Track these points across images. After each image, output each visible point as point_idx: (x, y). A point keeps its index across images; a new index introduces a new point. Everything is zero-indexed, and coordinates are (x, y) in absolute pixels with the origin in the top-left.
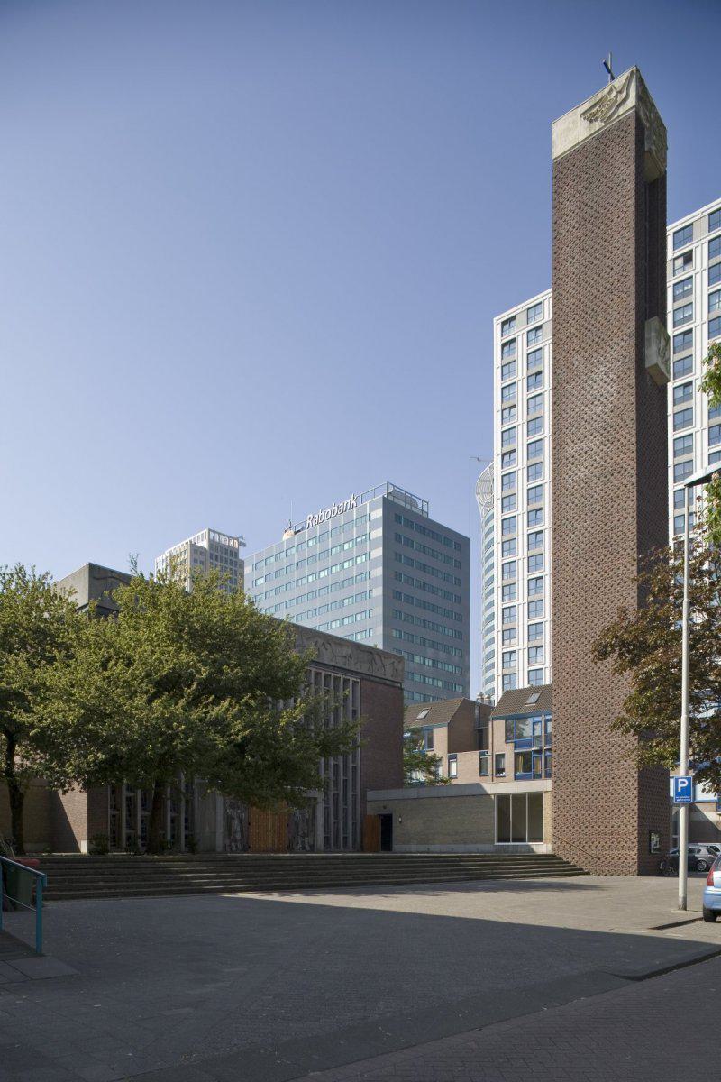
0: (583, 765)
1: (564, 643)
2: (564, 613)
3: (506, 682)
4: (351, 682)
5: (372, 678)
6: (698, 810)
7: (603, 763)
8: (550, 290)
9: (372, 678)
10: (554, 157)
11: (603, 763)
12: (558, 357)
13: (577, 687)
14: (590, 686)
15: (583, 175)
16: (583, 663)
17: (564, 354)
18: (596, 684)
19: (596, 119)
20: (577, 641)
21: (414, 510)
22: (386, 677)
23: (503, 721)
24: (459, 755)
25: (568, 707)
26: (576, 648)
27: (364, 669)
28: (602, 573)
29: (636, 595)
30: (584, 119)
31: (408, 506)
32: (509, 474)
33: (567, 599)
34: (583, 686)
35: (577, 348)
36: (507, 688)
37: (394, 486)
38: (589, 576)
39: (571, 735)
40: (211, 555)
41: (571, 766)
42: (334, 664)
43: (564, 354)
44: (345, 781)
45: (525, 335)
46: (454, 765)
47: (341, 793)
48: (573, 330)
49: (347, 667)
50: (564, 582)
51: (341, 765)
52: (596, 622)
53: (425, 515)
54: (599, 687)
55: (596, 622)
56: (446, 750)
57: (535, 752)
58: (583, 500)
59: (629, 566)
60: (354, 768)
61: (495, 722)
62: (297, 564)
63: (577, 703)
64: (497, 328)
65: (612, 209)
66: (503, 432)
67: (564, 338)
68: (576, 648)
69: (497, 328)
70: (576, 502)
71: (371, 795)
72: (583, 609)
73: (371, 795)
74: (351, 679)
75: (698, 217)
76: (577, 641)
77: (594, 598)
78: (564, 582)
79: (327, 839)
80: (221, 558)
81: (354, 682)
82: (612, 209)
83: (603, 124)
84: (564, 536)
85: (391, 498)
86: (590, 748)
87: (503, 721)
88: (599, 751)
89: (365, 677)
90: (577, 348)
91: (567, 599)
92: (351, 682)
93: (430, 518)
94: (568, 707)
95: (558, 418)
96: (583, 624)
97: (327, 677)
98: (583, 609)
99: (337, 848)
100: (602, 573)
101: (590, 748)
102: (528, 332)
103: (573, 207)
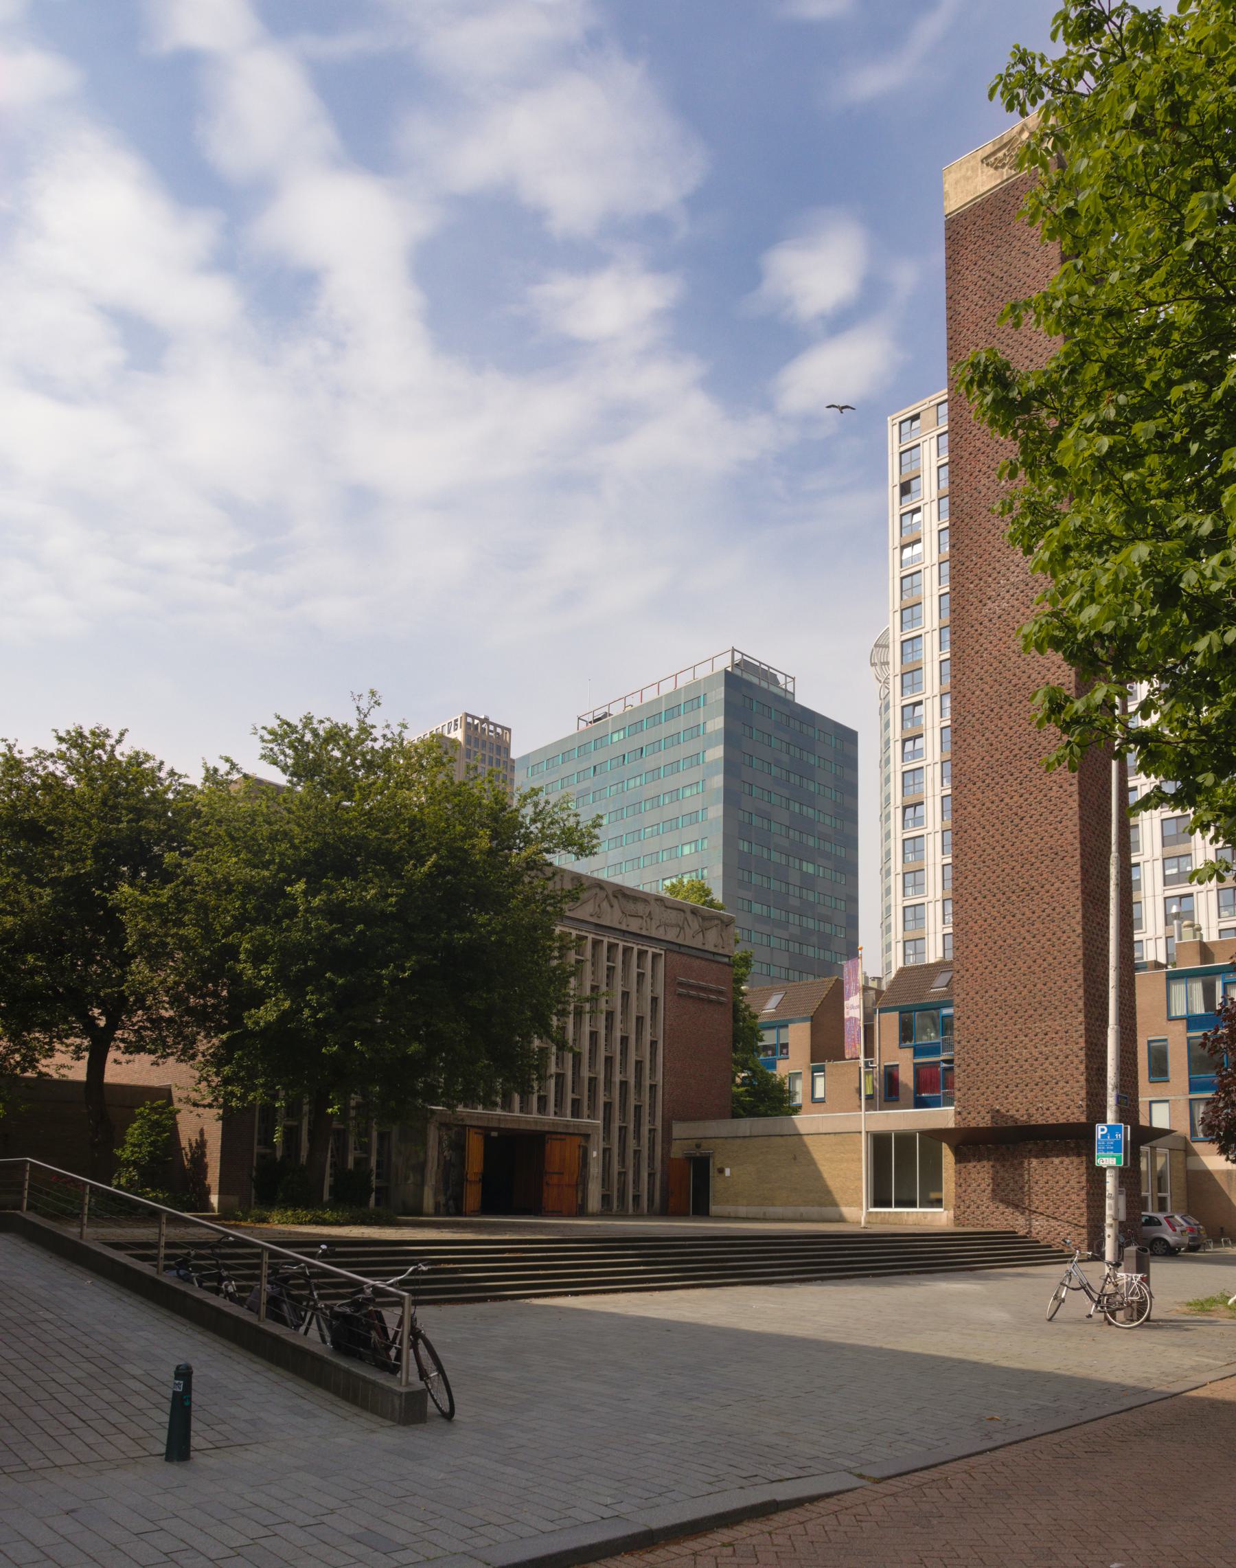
0: (1002, 1087)
1: (970, 900)
2: (970, 854)
3: (909, 952)
4: (650, 955)
5: (682, 950)
6: (1195, 1154)
7: (1032, 1085)
8: (946, 390)
9: (682, 950)
10: (947, 212)
11: (1032, 1085)
12: (958, 481)
13: (991, 968)
14: (1010, 965)
15: (988, 237)
16: (999, 930)
17: (966, 477)
18: (1020, 963)
19: (1004, 166)
20: (989, 897)
21: (773, 689)
22: (706, 948)
23: (896, 1014)
24: (828, 1065)
25: (977, 998)
26: (988, 908)
27: (671, 935)
28: (1026, 796)
29: (1077, 828)
30: (987, 165)
31: (764, 684)
32: (912, 639)
33: (974, 834)
34: (1000, 966)
35: (984, 469)
36: (911, 961)
37: (743, 654)
38: (1007, 800)
39: (982, 1041)
40: (468, 751)
41: (983, 1089)
42: (624, 927)
43: (966, 477)
44: (638, 1108)
45: (934, 441)
46: (820, 1083)
47: (631, 1127)
48: (978, 444)
49: (644, 932)
50: (970, 808)
51: (632, 1081)
52: (1018, 868)
53: (789, 697)
54: (1024, 968)
55: (1018, 868)
56: (808, 1058)
57: (945, 1061)
58: (996, 687)
59: (1065, 786)
60: (653, 1087)
61: (883, 1015)
62: (595, 767)
63: (991, 992)
64: (893, 433)
65: (1029, 280)
66: (902, 578)
67: (966, 455)
68: (988, 908)
69: (893, 433)
70: (987, 689)
71: (679, 1130)
72: (998, 849)
73: (679, 1130)
74: (651, 950)
75: (925, 407)
76: (989, 897)
77: (1016, 832)
78: (970, 808)
79: (606, 1199)
80: (491, 750)
81: (655, 956)
82: (1029, 280)
83: (1013, 172)
84: (969, 740)
85: (738, 672)
86: (1012, 1062)
87: (896, 1014)
88: (1026, 1066)
89: (674, 948)
90: (984, 469)
91: (974, 834)
92: (650, 955)
93: (796, 701)
94: (977, 998)
95: (959, 567)
96: (998, 872)
97: (612, 947)
98: (998, 849)
99: (623, 1215)
100: (1026, 796)
101: (1012, 1062)
102: (939, 436)
103: (975, 279)
